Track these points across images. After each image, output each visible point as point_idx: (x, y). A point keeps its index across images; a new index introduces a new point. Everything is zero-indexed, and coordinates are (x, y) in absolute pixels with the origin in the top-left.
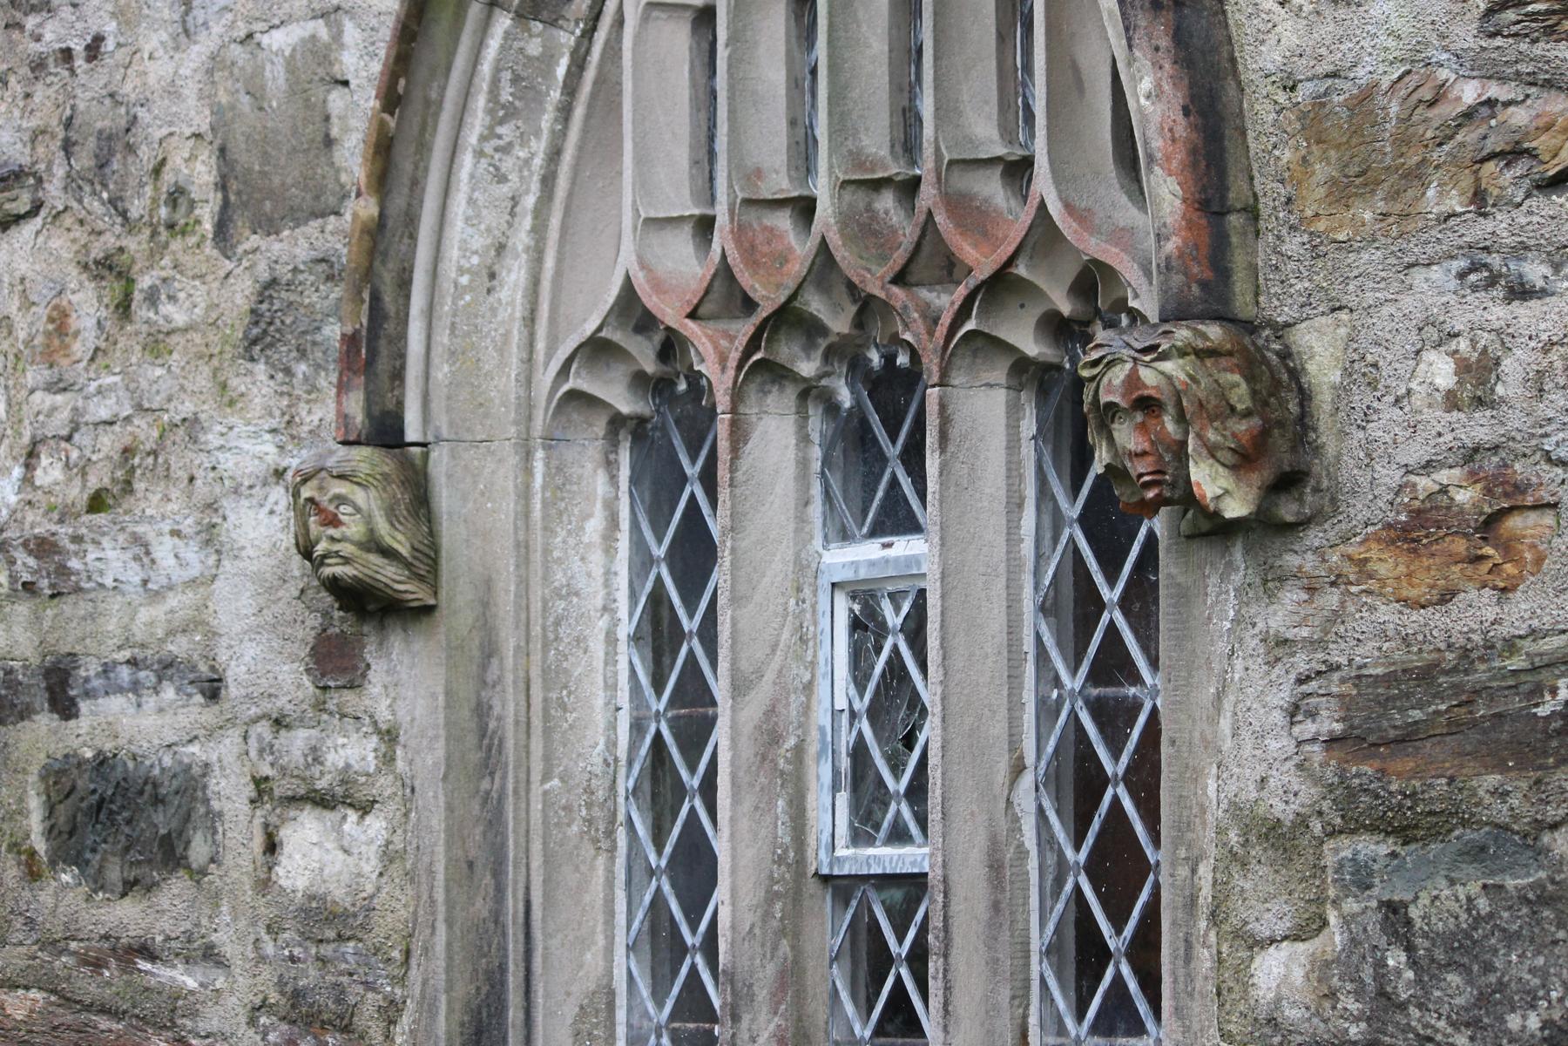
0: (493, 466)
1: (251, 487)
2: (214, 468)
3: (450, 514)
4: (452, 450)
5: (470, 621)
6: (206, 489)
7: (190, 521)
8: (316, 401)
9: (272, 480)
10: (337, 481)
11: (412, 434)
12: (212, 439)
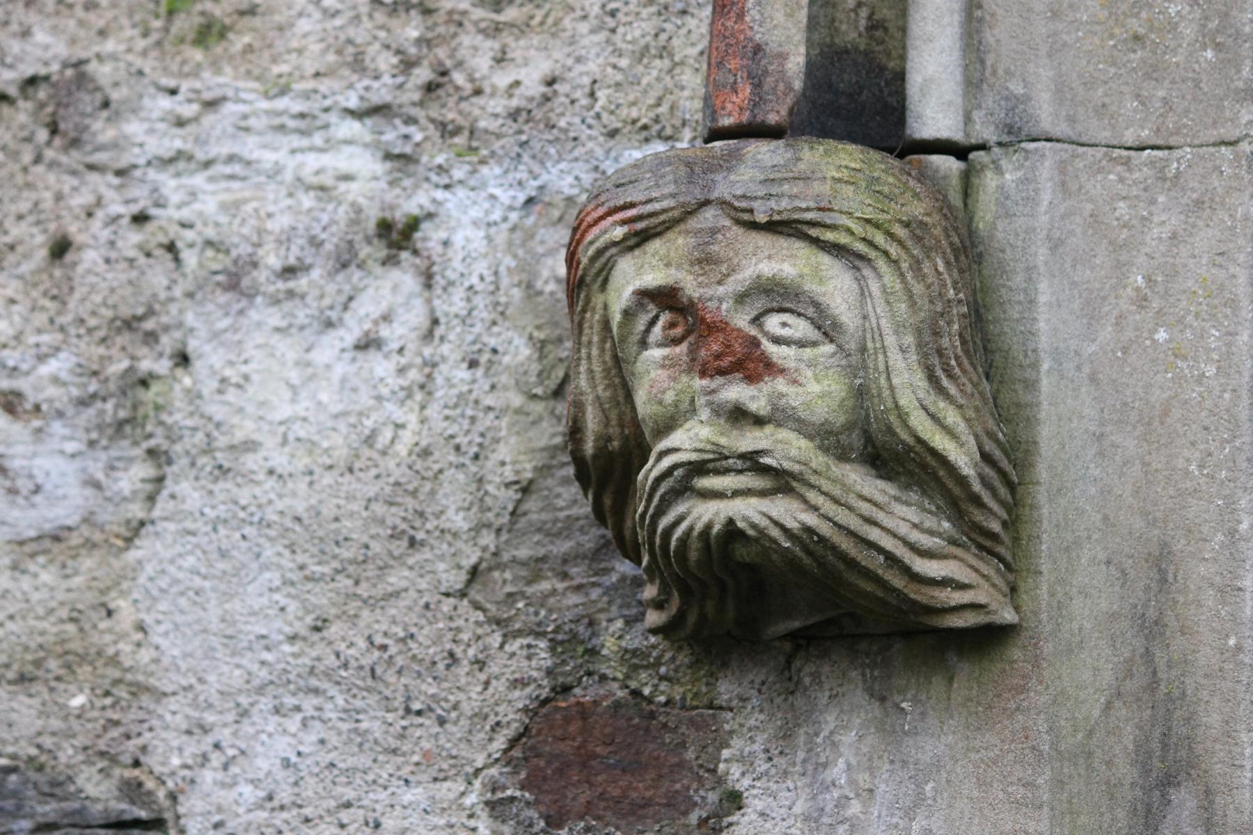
0: (1175, 221)
1: (289, 272)
2: (140, 219)
3: (1057, 355)
4: (1062, 167)
5: (1107, 677)
6: (118, 276)
7: (58, 365)
8: (522, 28)
9: (372, 251)
11: (935, 111)
12: (144, 132)
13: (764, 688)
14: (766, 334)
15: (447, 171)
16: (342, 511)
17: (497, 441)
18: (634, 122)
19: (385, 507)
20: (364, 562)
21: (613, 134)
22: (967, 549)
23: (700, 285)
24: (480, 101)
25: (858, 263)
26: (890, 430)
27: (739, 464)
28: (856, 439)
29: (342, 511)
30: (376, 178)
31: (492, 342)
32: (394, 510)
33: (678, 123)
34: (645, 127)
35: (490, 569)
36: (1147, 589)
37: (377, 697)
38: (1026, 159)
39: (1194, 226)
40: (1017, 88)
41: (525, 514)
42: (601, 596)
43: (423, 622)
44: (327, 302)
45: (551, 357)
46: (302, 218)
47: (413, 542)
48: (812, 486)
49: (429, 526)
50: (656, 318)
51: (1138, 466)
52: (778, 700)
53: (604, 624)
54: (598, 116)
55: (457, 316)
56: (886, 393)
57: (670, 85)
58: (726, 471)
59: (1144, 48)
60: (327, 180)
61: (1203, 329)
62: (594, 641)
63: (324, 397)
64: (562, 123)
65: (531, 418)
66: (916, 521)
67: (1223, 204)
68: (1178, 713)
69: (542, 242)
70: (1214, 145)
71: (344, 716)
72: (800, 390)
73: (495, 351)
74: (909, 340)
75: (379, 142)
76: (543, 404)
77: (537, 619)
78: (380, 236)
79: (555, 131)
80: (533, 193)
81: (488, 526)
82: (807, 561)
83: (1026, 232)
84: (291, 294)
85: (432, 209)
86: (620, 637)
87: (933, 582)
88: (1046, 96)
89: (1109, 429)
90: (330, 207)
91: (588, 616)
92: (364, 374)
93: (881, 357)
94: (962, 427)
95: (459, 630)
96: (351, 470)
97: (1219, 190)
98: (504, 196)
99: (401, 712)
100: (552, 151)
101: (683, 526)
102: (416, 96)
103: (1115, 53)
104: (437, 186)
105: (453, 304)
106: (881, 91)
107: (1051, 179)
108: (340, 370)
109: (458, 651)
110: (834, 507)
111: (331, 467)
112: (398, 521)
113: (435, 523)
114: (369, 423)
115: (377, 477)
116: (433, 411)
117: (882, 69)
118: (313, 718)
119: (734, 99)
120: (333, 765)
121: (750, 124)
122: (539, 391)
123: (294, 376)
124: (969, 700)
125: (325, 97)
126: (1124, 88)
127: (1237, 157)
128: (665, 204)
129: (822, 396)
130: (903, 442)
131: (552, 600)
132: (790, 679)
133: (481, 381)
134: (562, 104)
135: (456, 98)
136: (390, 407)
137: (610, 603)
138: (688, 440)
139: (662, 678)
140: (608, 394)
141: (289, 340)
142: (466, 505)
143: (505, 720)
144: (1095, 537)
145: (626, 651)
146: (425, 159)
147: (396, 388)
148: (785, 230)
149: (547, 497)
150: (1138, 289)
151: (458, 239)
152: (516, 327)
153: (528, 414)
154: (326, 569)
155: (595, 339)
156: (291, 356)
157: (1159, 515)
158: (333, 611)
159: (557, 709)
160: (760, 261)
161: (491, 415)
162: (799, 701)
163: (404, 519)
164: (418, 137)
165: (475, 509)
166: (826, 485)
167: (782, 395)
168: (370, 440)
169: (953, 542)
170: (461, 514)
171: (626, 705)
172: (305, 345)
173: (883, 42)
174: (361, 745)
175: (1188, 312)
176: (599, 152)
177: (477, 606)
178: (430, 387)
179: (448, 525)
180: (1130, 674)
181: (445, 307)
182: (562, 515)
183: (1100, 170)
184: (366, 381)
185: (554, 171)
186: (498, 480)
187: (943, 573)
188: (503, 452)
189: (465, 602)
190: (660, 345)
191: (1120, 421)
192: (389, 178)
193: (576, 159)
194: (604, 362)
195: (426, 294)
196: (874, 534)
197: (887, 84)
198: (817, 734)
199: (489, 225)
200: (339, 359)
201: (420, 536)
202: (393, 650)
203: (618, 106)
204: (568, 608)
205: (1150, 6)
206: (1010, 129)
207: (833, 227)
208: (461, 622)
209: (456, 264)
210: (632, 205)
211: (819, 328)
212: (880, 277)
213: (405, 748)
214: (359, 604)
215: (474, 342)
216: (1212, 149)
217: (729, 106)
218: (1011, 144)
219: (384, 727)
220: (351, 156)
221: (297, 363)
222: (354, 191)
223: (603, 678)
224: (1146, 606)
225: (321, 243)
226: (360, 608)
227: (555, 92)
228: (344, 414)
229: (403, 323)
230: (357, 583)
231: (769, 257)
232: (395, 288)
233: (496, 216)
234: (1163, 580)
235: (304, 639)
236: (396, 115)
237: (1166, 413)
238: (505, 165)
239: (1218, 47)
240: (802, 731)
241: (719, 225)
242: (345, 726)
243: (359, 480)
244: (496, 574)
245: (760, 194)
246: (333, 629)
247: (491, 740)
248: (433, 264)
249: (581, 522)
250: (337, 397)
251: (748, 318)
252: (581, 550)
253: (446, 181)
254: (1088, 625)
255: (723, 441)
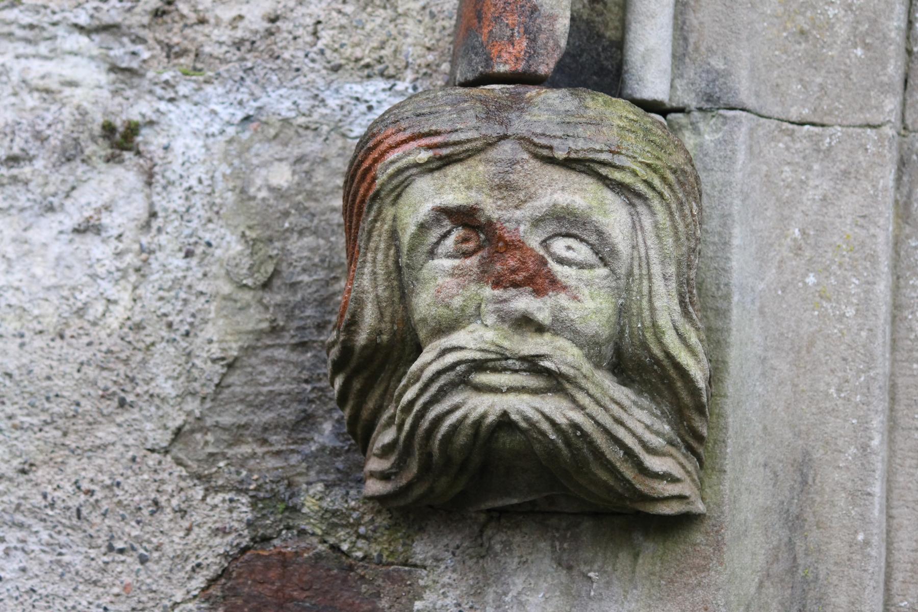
0: (826, 186)
4: (752, 131)
5: (761, 560)
9: (97, 149)
10: (557, 174)
11: (653, 77)
13: (458, 552)
14: (552, 255)
15: (173, 87)
16: (55, 371)
17: (205, 321)
18: (357, 60)
19: (97, 372)
20: (74, 416)
21: (336, 69)
22: (679, 449)
23: (499, 208)
24: (206, 29)
25: (635, 201)
26: (644, 346)
27: (518, 365)
28: (608, 351)
29: (55, 371)
30: (100, 87)
31: (207, 237)
32: (105, 374)
33: (401, 65)
34: (367, 66)
35: (193, 431)
36: (792, 488)
37: (82, 535)
38: (724, 124)
39: (840, 192)
40: (718, 63)
41: (229, 386)
42: (300, 462)
43: (130, 473)
44: (51, 189)
45: (261, 253)
46: (24, 114)
47: (122, 403)
48: (582, 389)
49: (138, 390)
50: (449, 233)
51: (789, 387)
52: (470, 563)
53: (304, 486)
54: (322, 52)
55: (175, 211)
56: (646, 313)
57: (394, 32)
58: (505, 369)
59: (807, 41)
60: (54, 86)
61: (845, 277)
62: (295, 500)
63: (38, 271)
64: (286, 55)
65: (239, 305)
66: (649, 423)
67: (866, 176)
68: (811, 594)
69: (257, 155)
70: (860, 126)
71: (47, 549)
72: (579, 305)
73: (209, 244)
74: (672, 270)
75: (108, 56)
76: (252, 293)
77: (239, 478)
78: (104, 137)
79: (279, 62)
80: (251, 113)
81: (193, 394)
82: (565, 451)
83: (722, 185)
84: (14, 179)
85: (154, 118)
86: (321, 499)
87: (656, 476)
88: (744, 73)
89: (770, 354)
90: (54, 108)
91: (288, 478)
92: (81, 254)
93: (645, 283)
94: (699, 348)
95: (163, 482)
96: (62, 337)
97: (864, 164)
98: (224, 113)
99: (103, 549)
100: (274, 78)
101: (458, 414)
102: (146, 20)
103: (787, 43)
104: (161, 99)
105: (175, 200)
106: (598, 55)
107: (744, 143)
108: (56, 249)
109: (162, 499)
110: (597, 407)
111: (41, 332)
112: (110, 384)
113: (146, 388)
114: (82, 297)
115: (90, 344)
116: (147, 291)
117: (600, 36)
118: (16, 548)
119: (511, 50)
120: (34, 591)
121: (524, 73)
122: (249, 282)
123: (11, 251)
124: (653, 574)
125: (54, 13)
126: (792, 73)
127: (881, 138)
128: (470, 135)
129: (597, 311)
130: (652, 356)
131: (252, 463)
132: (482, 545)
133: (195, 269)
134: (285, 39)
135: (181, 24)
136: (104, 285)
137: (308, 468)
138: (472, 340)
139: (359, 536)
140: (386, 294)
141: (8, 219)
142: (175, 374)
143: (205, 563)
144: (758, 443)
145: (326, 511)
146: (150, 74)
147: (113, 269)
148: (578, 167)
149: (251, 374)
150: (795, 240)
151: (178, 146)
152: (228, 226)
153: (235, 301)
154: (35, 421)
155: (382, 246)
156: (9, 233)
157: (803, 428)
158: (41, 457)
159: (259, 556)
160: (554, 192)
161: (202, 299)
162: (489, 564)
163: (115, 382)
164: (146, 55)
165: (182, 379)
166: (592, 390)
167: (562, 309)
168: (80, 312)
169: (671, 443)
170: (170, 382)
171: (327, 558)
172: (24, 225)
173: (602, 14)
174: (62, 575)
175: (833, 261)
176: (321, 83)
177: (179, 462)
178: (145, 270)
179: (157, 391)
180: (776, 559)
181: (164, 203)
182: (265, 390)
183: (773, 139)
184: (81, 261)
185: (273, 95)
186: (205, 355)
187: (665, 469)
188: (210, 332)
189: (169, 458)
190: (449, 256)
191: (778, 348)
192: (112, 88)
193: (296, 87)
194: (387, 266)
195: (147, 190)
196: (621, 433)
197: (604, 49)
198: (505, 594)
199: (207, 135)
200: (57, 239)
201: (130, 398)
202: (99, 495)
203: (342, 46)
204: (268, 470)
205: (814, 8)
206: (709, 98)
207: (621, 168)
208: (165, 476)
209: (176, 166)
210: (437, 133)
211: (597, 254)
212: (653, 214)
213: (105, 581)
214: (67, 452)
215: (191, 236)
216: (859, 130)
217: (505, 56)
218: (711, 110)
219: (86, 561)
220: (75, 66)
221: (14, 240)
222: (79, 96)
223: (302, 533)
224: (790, 503)
225: (47, 138)
226: (68, 456)
227: (278, 28)
228: (56, 287)
229: (122, 214)
230: (65, 434)
231: (563, 189)
232: (118, 182)
233: (215, 128)
234: (805, 482)
235: (11, 480)
236: (124, 35)
237: (812, 344)
238: (228, 86)
239: (867, 47)
240: (491, 590)
241: (519, 157)
242: (47, 558)
243: (69, 345)
244: (198, 436)
245: (560, 134)
246: (40, 473)
247: (190, 578)
248: (155, 165)
249: (283, 397)
250: (51, 272)
251: (539, 240)
252: (282, 421)
253: (172, 95)
254: (750, 517)
255: (506, 344)
